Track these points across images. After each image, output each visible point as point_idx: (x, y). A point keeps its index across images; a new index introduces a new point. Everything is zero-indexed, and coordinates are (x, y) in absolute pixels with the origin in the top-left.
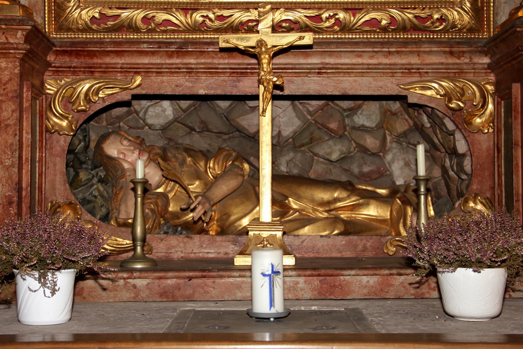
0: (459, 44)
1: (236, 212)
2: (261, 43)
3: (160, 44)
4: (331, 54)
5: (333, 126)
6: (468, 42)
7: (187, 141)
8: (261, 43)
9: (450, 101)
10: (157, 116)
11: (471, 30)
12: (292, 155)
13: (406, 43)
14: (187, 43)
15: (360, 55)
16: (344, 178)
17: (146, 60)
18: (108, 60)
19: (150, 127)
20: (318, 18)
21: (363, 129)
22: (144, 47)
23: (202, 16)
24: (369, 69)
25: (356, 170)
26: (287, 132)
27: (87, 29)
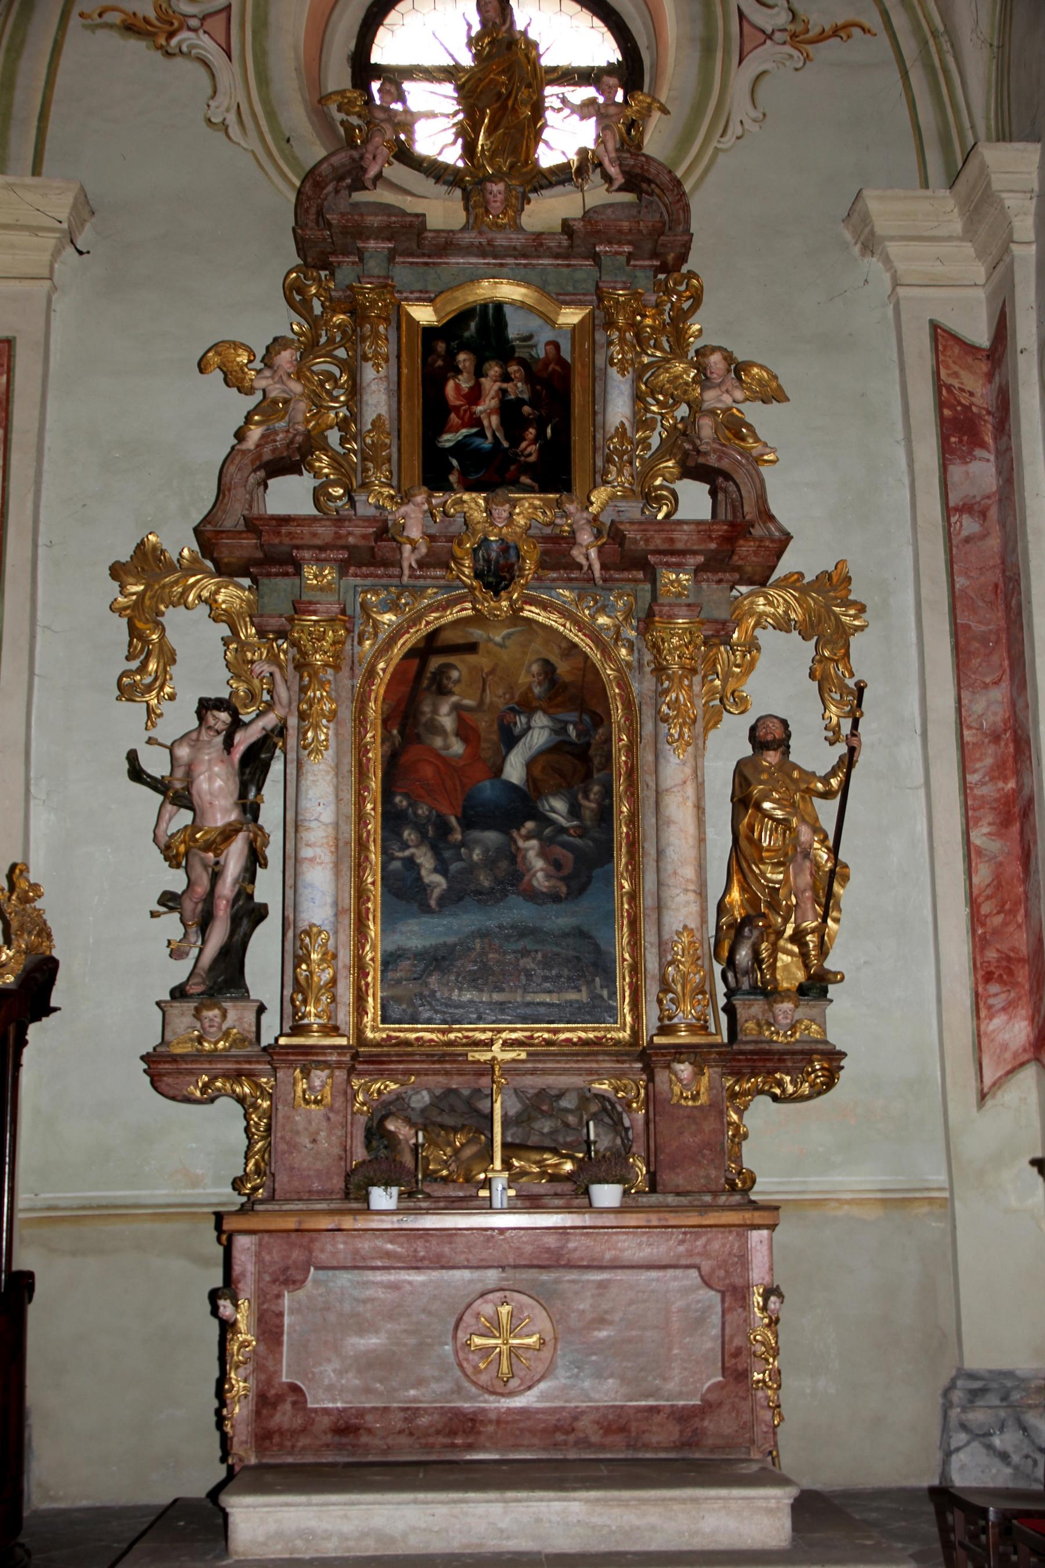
0: (622, 1055)
1: (476, 1168)
2: (494, 1058)
3: (428, 1055)
4: (540, 1061)
5: (545, 1108)
6: (627, 1054)
7: (439, 1119)
8: (494, 1058)
9: (617, 1092)
10: (418, 1101)
11: (631, 1045)
12: (515, 1129)
13: (588, 1054)
14: (444, 1055)
15: (558, 1062)
16: (553, 1145)
17: (417, 1066)
18: (392, 1066)
19: (413, 1109)
20: (531, 1037)
21: (567, 1110)
22: (417, 1058)
23: (271, 674)
24: (565, 1072)
25: (561, 1140)
26: (512, 1112)
27: (378, 1045)
